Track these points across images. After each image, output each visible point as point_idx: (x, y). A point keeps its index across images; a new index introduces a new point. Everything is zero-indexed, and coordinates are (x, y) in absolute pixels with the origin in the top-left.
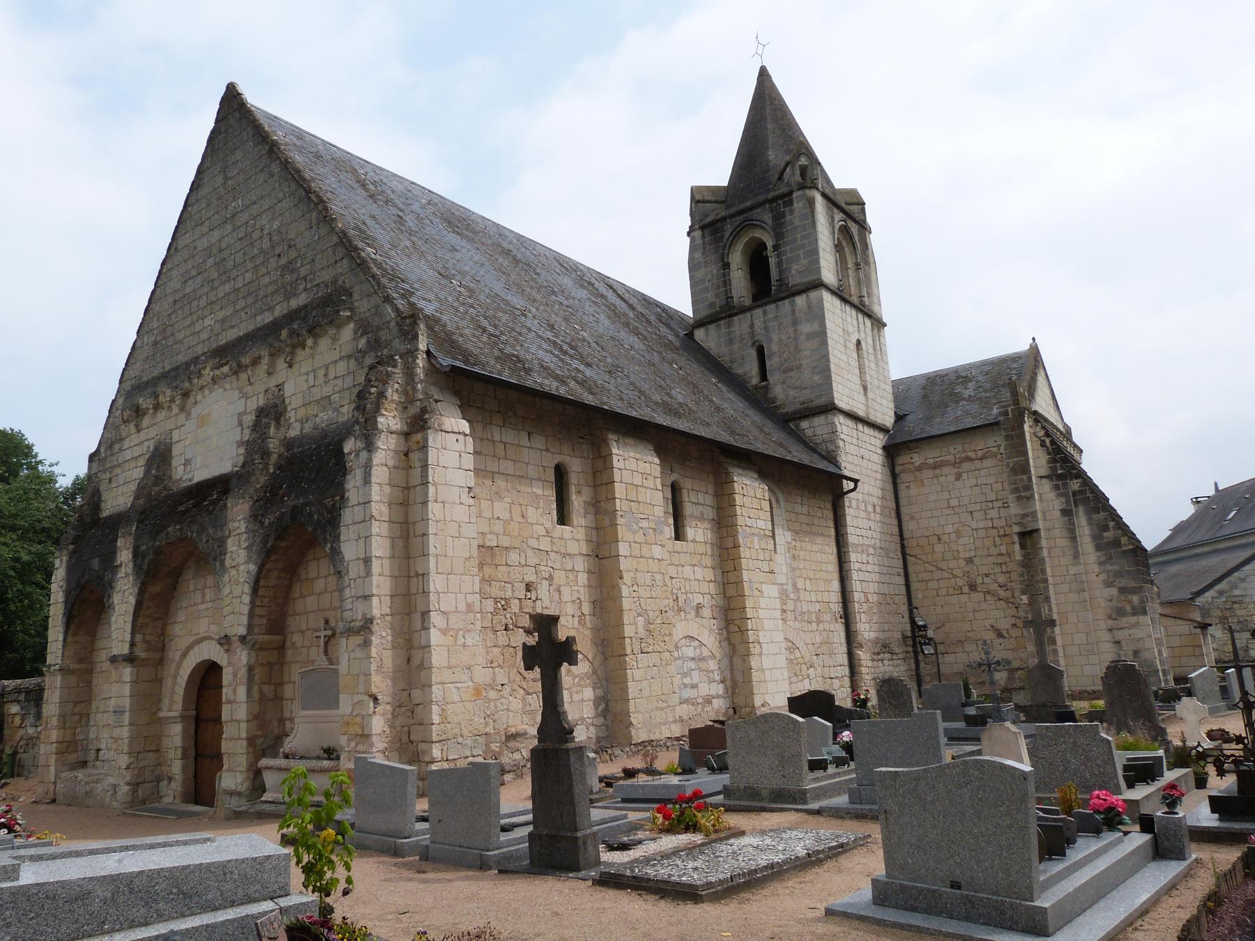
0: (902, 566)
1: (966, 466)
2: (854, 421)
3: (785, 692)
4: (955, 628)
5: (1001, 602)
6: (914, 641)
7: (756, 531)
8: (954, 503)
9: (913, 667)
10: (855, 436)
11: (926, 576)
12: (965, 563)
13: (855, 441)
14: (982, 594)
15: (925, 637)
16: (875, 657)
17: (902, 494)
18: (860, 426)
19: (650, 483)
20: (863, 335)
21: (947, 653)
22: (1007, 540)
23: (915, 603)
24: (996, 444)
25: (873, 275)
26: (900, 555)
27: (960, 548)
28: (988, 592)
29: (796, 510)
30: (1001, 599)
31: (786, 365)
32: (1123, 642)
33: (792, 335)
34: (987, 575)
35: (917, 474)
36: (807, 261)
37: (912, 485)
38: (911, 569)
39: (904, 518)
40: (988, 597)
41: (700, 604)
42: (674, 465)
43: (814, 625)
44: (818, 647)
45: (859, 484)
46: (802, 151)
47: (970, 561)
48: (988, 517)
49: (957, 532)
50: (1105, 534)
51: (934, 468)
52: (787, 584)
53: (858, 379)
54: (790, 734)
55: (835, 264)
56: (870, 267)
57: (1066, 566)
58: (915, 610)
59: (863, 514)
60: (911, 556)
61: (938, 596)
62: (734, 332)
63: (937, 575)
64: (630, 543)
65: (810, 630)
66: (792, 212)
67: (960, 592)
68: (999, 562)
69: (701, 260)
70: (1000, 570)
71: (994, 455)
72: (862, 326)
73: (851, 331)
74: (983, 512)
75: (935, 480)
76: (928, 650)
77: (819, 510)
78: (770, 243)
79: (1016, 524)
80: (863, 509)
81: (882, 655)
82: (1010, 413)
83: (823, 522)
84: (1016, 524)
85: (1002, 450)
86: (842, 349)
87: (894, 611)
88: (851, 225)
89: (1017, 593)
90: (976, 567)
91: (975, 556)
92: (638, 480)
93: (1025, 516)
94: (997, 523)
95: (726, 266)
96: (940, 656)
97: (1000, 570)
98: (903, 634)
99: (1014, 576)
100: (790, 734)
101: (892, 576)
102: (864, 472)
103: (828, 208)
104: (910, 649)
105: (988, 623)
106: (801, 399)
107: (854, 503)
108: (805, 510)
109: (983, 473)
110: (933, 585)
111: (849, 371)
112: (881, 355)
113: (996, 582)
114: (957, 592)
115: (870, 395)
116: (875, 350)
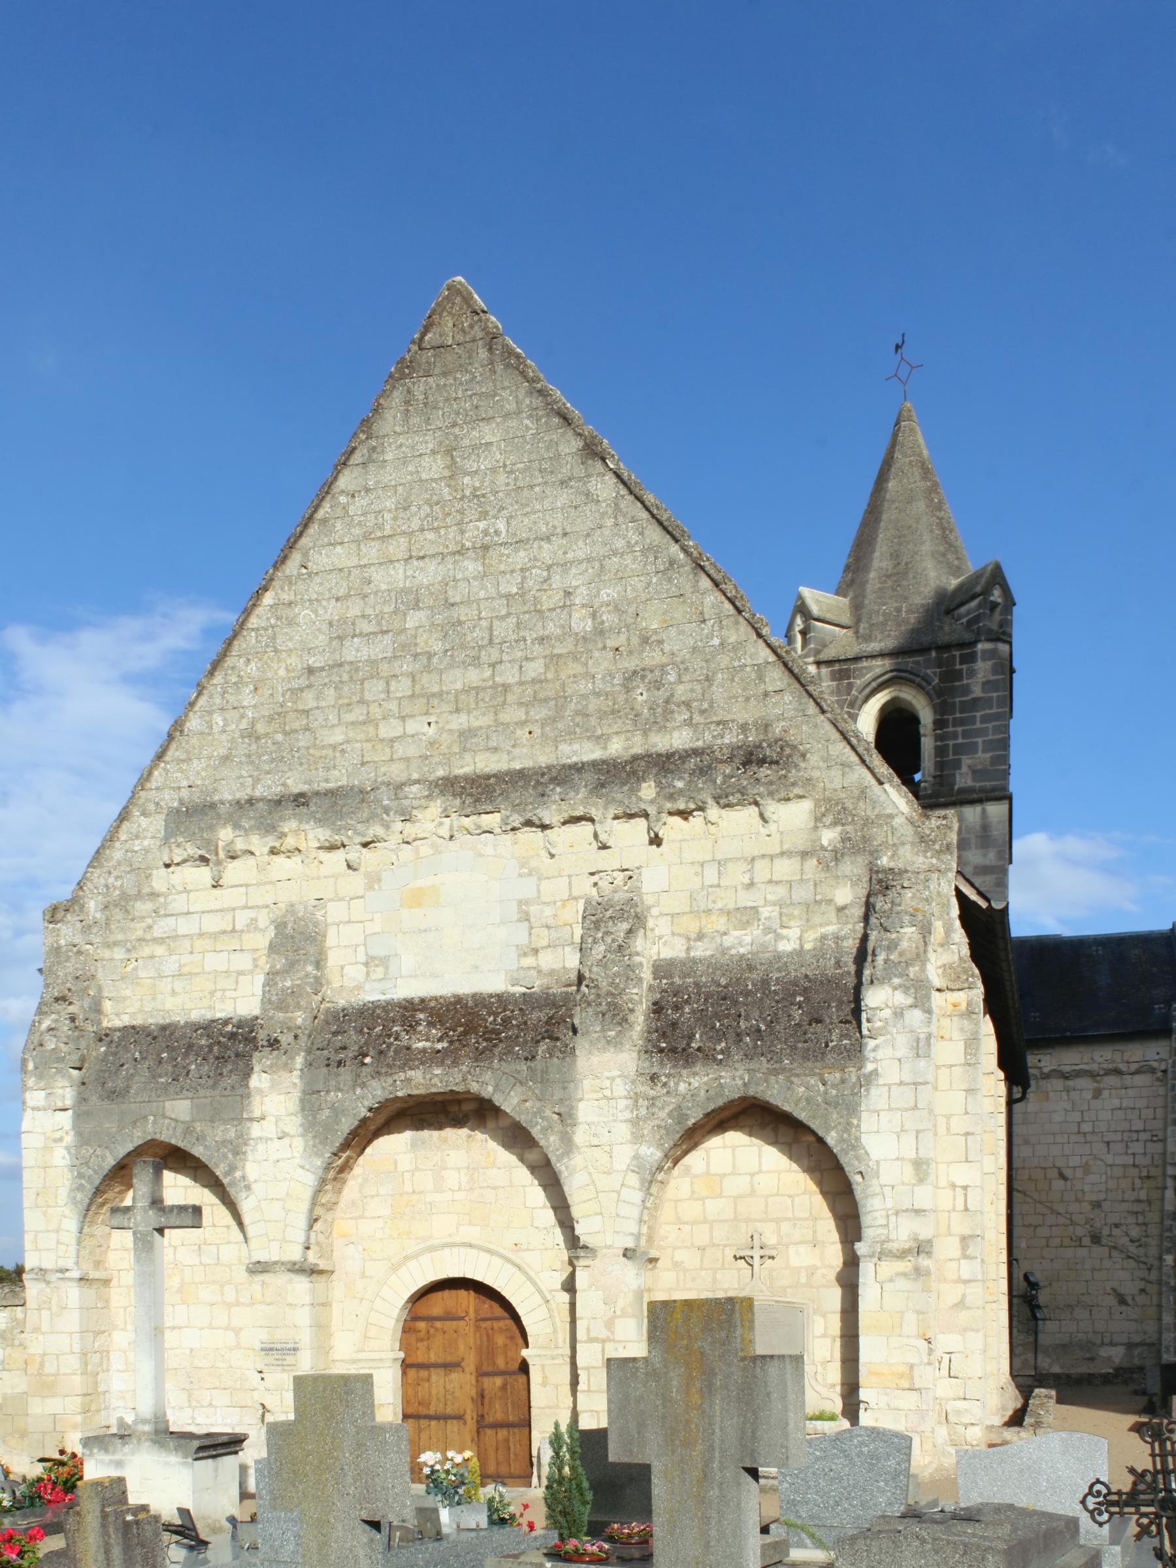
1: (1112, 1080)
5: (1130, 1260)
8: (1086, 1127)
12: (1089, 1207)
14: (1107, 1249)
27: (1087, 1188)
28: (1115, 1248)
34: (1117, 1226)
36: (988, 755)
40: (1115, 1253)
47: (1097, 1205)
48: (1130, 1151)
63: (1051, 1219)
66: (972, 673)
68: (1135, 1209)
70: (1134, 1221)
78: (926, 716)
94: (1140, 1160)
109: (1131, 1092)
110: (1043, 1232)
113: (1127, 1235)
114: (1074, 1244)
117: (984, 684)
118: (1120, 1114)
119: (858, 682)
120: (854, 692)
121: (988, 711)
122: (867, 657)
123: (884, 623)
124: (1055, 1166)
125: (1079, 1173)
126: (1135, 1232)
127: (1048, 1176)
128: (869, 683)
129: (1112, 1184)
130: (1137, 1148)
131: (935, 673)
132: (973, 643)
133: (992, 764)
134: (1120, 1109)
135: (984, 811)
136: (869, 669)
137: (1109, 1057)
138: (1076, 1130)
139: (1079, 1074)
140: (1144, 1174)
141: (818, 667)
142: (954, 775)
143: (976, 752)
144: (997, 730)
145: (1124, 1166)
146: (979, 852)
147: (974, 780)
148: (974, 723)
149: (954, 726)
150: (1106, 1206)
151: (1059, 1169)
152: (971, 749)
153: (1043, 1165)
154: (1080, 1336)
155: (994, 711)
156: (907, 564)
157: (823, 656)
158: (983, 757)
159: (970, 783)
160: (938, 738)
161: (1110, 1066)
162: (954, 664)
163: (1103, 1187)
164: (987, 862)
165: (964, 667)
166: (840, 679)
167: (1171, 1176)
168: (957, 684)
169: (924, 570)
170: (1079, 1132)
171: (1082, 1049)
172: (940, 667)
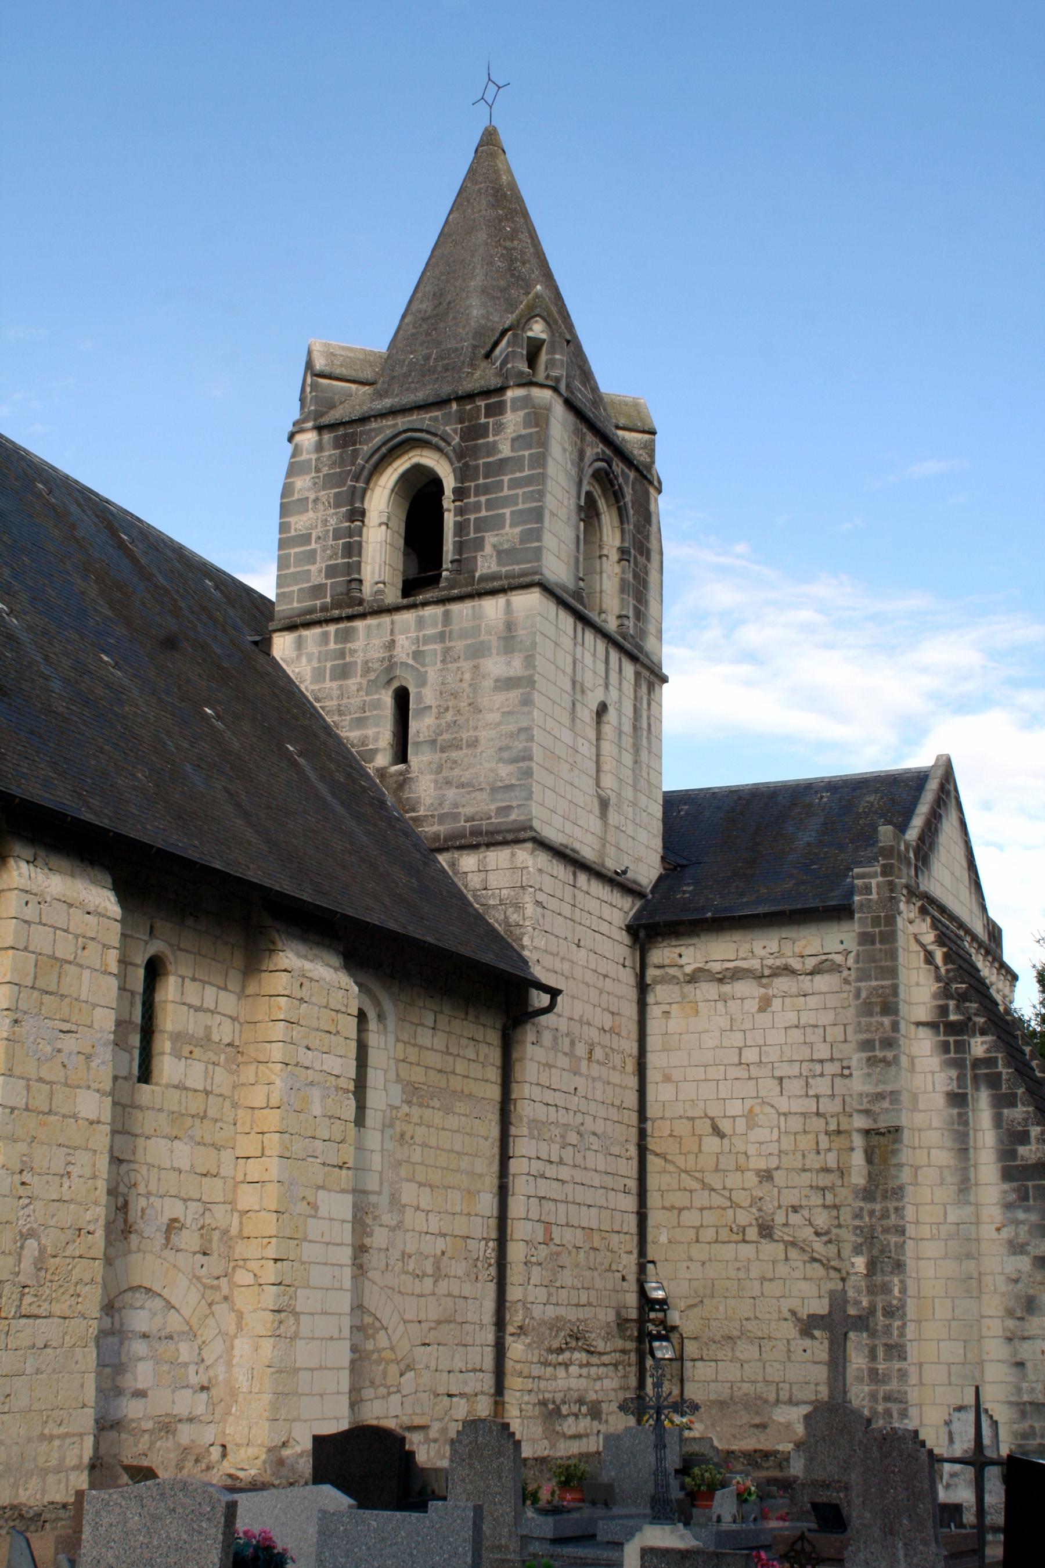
0: (634, 1173)
1: (782, 983)
2: (570, 869)
3: (337, 1419)
4: (722, 1308)
5: (816, 1265)
6: (641, 1329)
7: (319, 1077)
8: (750, 1055)
9: (633, 1382)
10: (568, 898)
11: (678, 1199)
12: (756, 1180)
13: (567, 910)
14: (781, 1246)
15: (663, 1322)
16: (552, 1358)
17: (654, 1026)
18: (582, 878)
19: (92, 955)
20: (614, 694)
21: (702, 1359)
22: (840, 1142)
23: (652, 1253)
24: (841, 948)
25: (653, 577)
26: (633, 1151)
27: (752, 1150)
28: (793, 1244)
29: (420, 1040)
30: (815, 1260)
31: (447, 736)
32: (1029, 1365)
33: (467, 676)
34: (795, 1209)
35: (688, 988)
36: (518, 530)
37: (675, 1009)
38: (652, 1182)
39: (653, 1075)
40: (793, 1253)
41: (175, 1220)
42: (158, 924)
43: (428, 1282)
44: (430, 1329)
45: (559, 999)
46: (538, 311)
47: (766, 1176)
48: (811, 1092)
49: (750, 1116)
50: (1022, 1150)
51: (721, 981)
52: (379, 1193)
53: (592, 782)
54: (204, 1525)
55: (573, 547)
56: (648, 559)
57: (944, 1205)
58: (650, 1266)
59: (563, 1062)
60: (657, 1155)
61: (697, 1241)
62: (353, 652)
63: (702, 1198)
64: (28, 1080)
65: (417, 1291)
66: (499, 428)
67: (740, 1237)
68: (821, 1184)
69: (307, 494)
70: (820, 1202)
71: (836, 968)
72: (614, 677)
73: (588, 684)
74: (803, 1082)
75: (720, 1005)
76: (664, 1351)
77: (472, 1043)
78: (449, 483)
79: (860, 1111)
80: (567, 1049)
81: (567, 1355)
82: (874, 890)
83: (476, 1071)
84: (860, 1111)
85: (851, 962)
86: (566, 719)
87: (606, 1266)
88: (618, 467)
89: (847, 1250)
90: (776, 1189)
91: (777, 1168)
92: (65, 949)
93: (879, 1096)
94: (826, 1106)
95: (358, 515)
96: (688, 1364)
97: (820, 1202)
98: (618, 1314)
99: (846, 1216)
100: (204, 1525)
101: (612, 1194)
102: (578, 972)
103: (577, 432)
104: (632, 1345)
105: (786, 1305)
106: (469, 811)
107: (547, 1037)
108: (439, 1041)
109: (812, 1001)
110: (691, 1218)
111: (573, 765)
112: (648, 738)
113: (811, 1224)
114: (735, 1237)
115: (613, 816)
116: (635, 728)
117: (513, 440)
118: (796, 1035)
119: (365, 448)
120: (360, 461)
121: (518, 475)
122: (375, 417)
123: (406, 375)
124: (706, 1116)
125: (741, 1124)
126: (822, 1219)
127: (698, 1132)
128: (379, 448)
129: (787, 1143)
130: (821, 1086)
131: (455, 431)
132: (502, 390)
133: (522, 542)
134: (797, 1027)
135: (508, 604)
136: (380, 430)
137: (775, 949)
138: (736, 1060)
139: (736, 975)
140: (833, 1127)
141: (320, 434)
142: (475, 558)
143: (503, 527)
144: (528, 497)
145: (804, 1115)
146: (501, 659)
147: (499, 563)
148: (502, 490)
149: (476, 496)
150: (779, 1177)
151: (712, 1119)
152: (494, 523)
153: (690, 1114)
154: (746, 1386)
155: (526, 473)
156: (449, 303)
157: (325, 420)
158: (510, 533)
159: (494, 568)
160: (460, 512)
161: (778, 962)
162: (478, 417)
163: (774, 1148)
164: (512, 673)
165: (491, 420)
166: (344, 446)
167: (859, 1131)
168: (481, 441)
169: (468, 307)
170: (740, 1064)
171: (737, 936)
172: (461, 422)
